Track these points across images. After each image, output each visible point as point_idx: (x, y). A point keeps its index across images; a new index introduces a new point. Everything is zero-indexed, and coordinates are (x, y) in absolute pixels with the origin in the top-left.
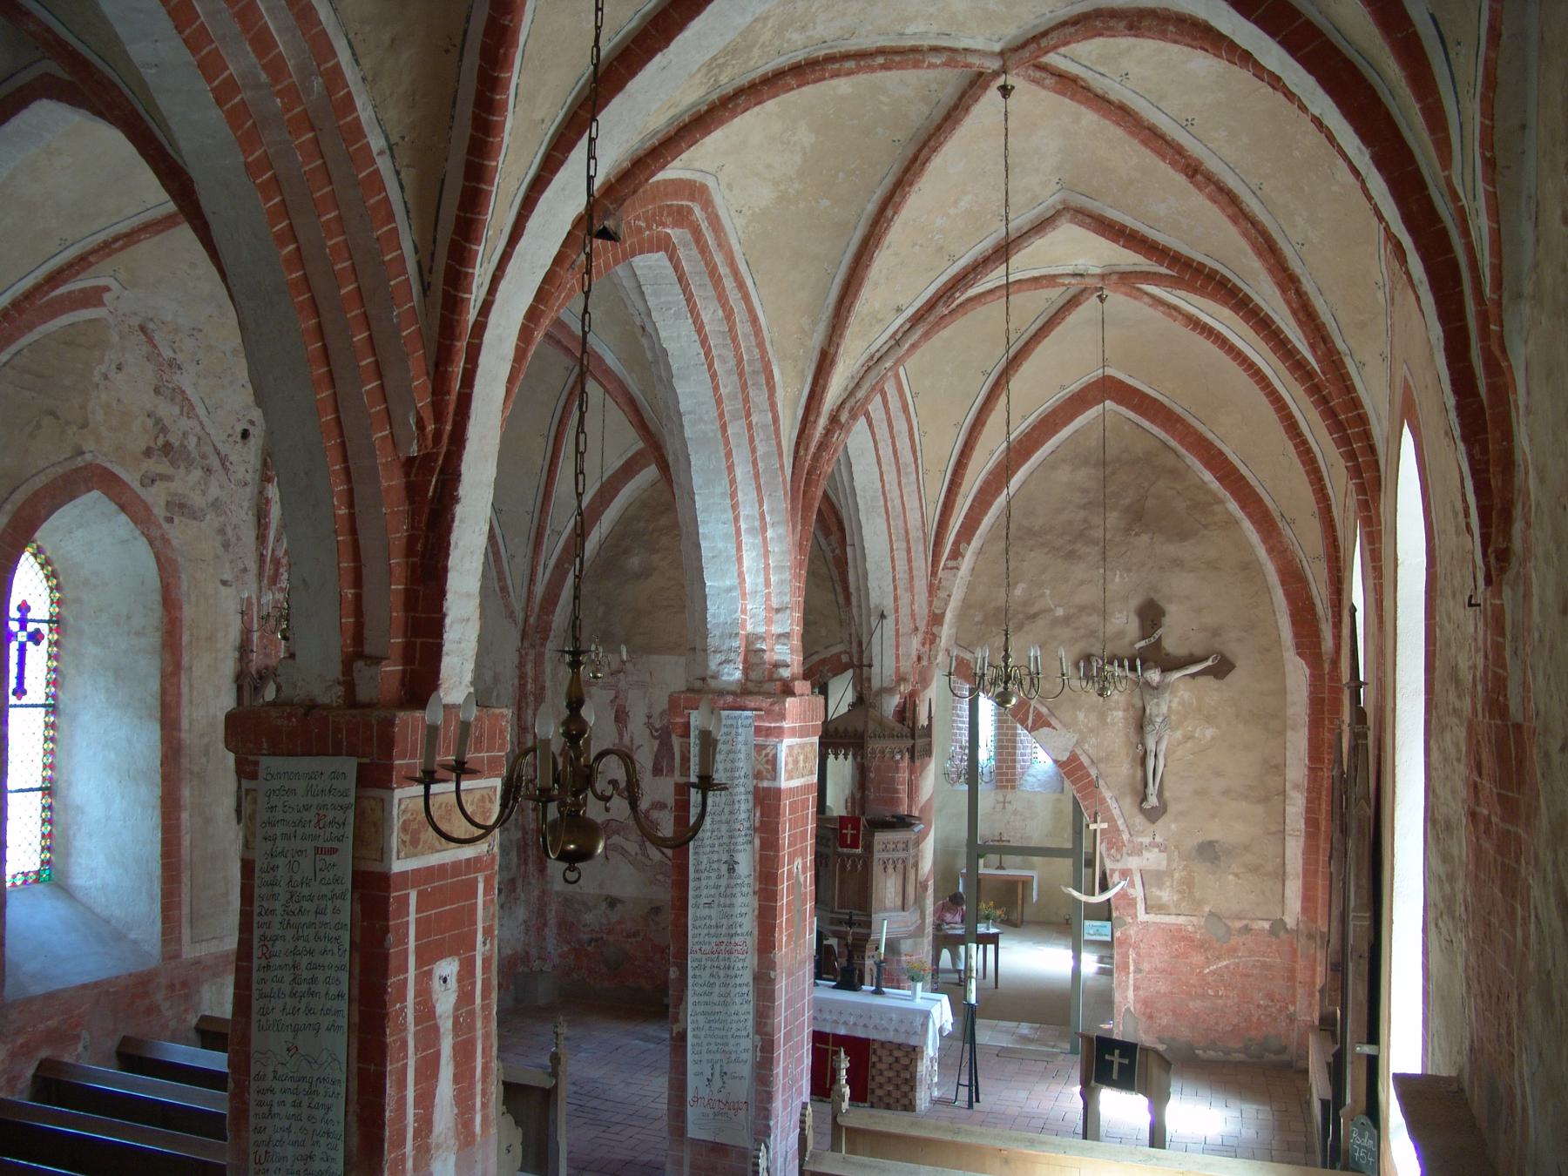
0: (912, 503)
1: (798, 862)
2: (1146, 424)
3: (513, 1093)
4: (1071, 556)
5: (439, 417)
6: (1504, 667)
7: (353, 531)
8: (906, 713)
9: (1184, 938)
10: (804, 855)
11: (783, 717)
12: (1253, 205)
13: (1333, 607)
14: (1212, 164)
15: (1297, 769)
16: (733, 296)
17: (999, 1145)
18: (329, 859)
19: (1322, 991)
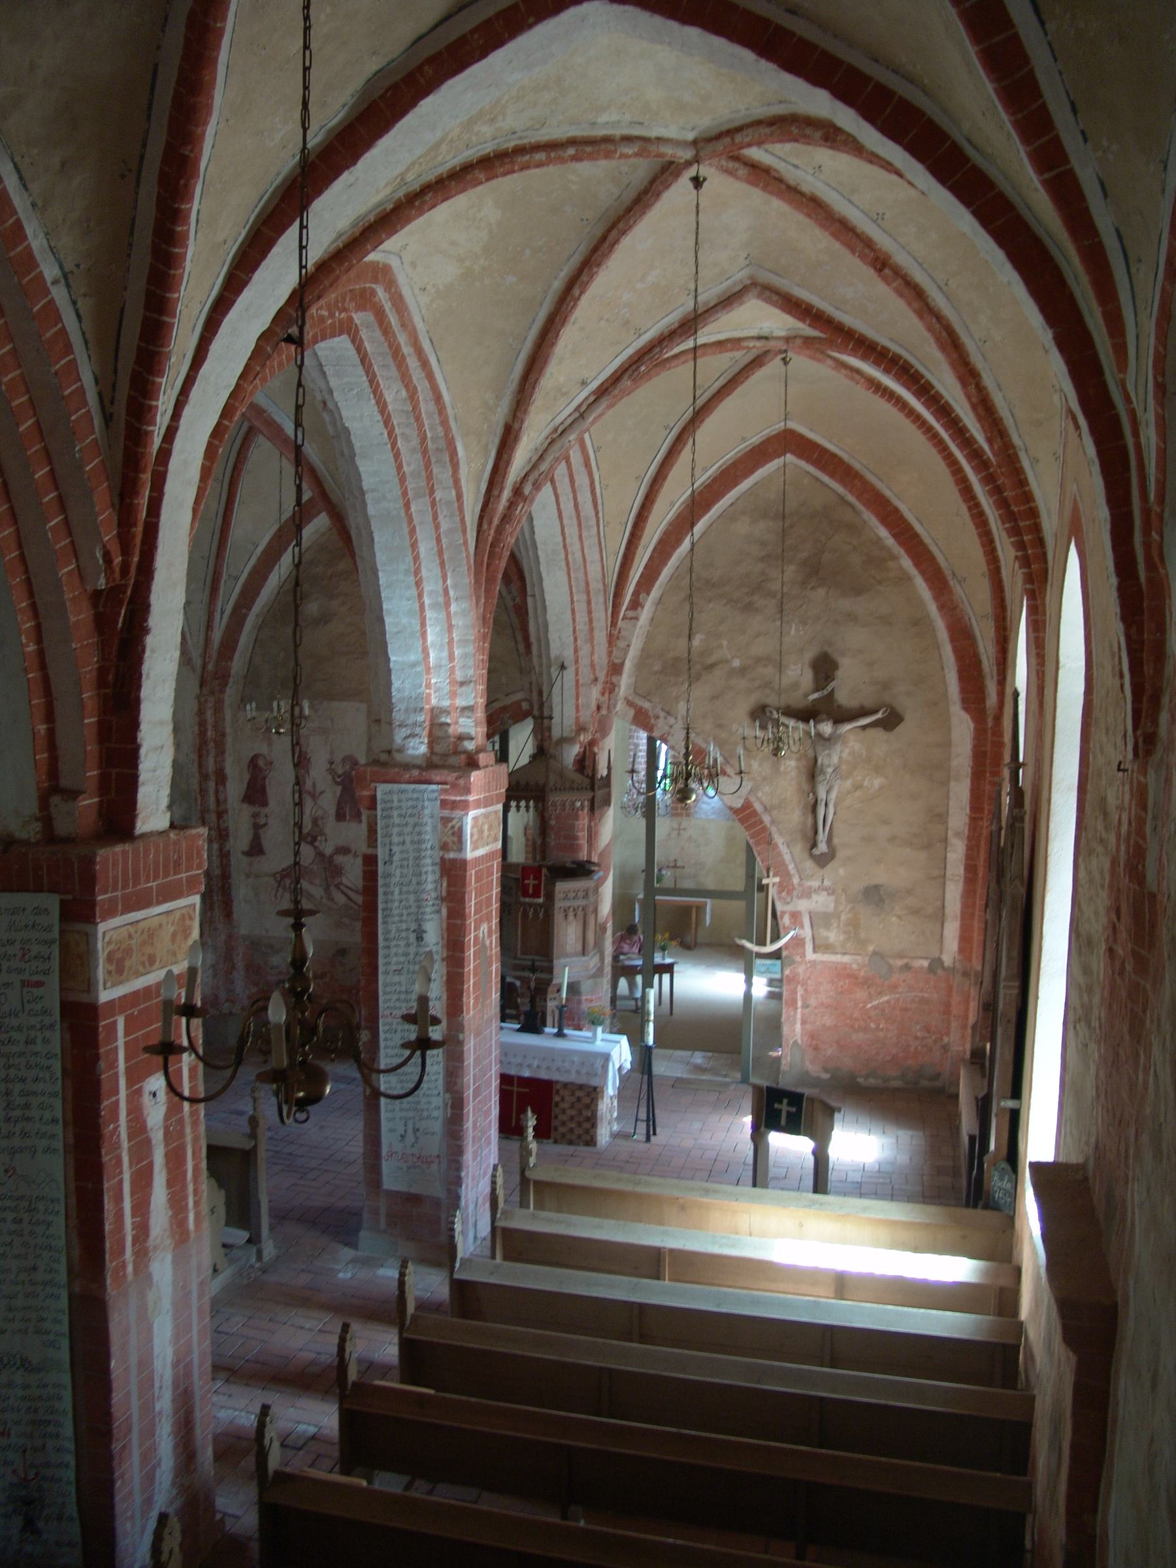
0: (593, 555)
1: (484, 927)
2: (826, 479)
3: (215, 1153)
4: (749, 608)
5: (126, 550)
6: (1144, 838)
7: (43, 666)
8: (585, 762)
9: (848, 976)
10: (489, 920)
11: (468, 791)
12: (939, 300)
13: (998, 665)
14: (901, 259)
15: (959, 818)
16: (417, 375)
17: (676, 1194)
18: (37, 992)
19: (974, 1027)
